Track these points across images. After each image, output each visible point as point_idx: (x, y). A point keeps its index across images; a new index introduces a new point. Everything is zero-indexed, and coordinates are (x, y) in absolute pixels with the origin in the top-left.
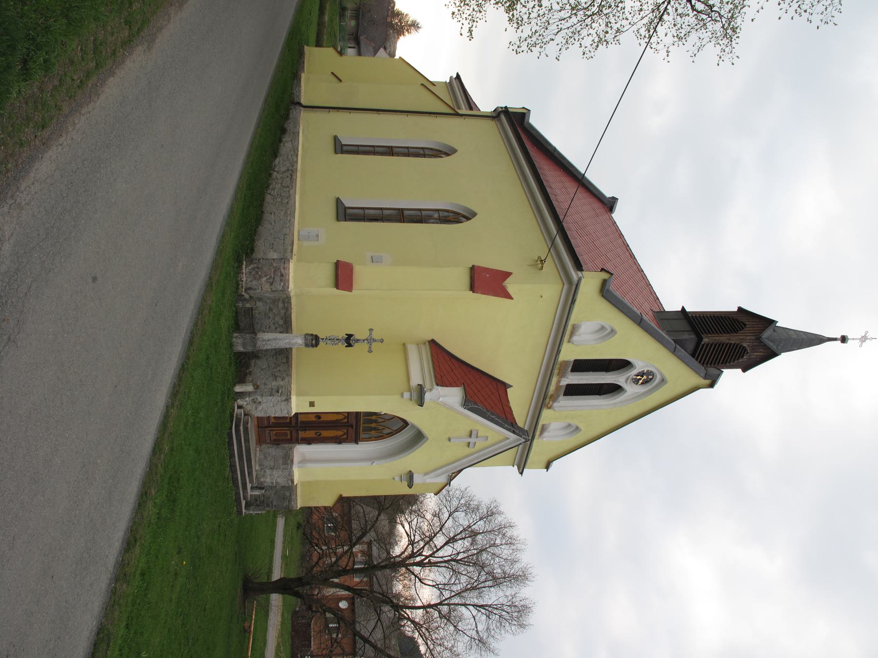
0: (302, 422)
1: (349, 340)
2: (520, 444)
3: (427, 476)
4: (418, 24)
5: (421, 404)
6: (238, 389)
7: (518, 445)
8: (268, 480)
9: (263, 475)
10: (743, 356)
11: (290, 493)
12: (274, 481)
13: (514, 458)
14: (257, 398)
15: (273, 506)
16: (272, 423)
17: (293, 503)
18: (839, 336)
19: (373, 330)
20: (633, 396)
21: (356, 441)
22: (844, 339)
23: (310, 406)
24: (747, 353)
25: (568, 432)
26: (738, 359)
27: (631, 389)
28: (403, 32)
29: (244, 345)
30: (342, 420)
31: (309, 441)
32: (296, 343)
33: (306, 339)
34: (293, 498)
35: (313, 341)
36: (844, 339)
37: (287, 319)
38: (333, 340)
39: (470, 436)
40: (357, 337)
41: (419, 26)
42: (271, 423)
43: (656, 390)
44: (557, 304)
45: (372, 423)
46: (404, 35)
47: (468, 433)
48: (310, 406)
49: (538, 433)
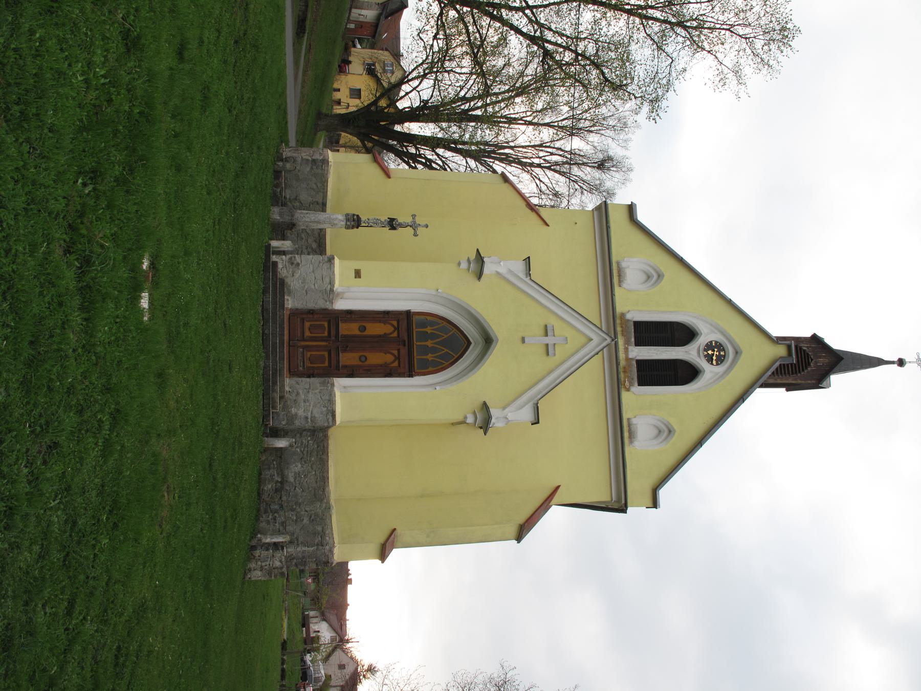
0: (344, 336)
1: (392, 224)
2: (604, 347)
3: (507, 410)
4: (374, 668)
5: (480, 275)
6: (274, 243)
7: (602, 349)
8: (301, 412)
9: (295, 400)
10: (809, 364)
11: (323, 528)
12: (309, 416)
13: (609, 486)
14: (295, 257)
15: (300, 542)
16: (307, 336)
17: (327, 538)
18: (896, 359)
19: (415, 216)
20: (715, 378)
21: (411, 376)
22: (901, 363)
23: (355, 278)
24: (812, 360)
25: (661, 440)
26: (806, 368)
27: (709, 371)
28: (360, 680)
29: (281, 214)
30: (391, 334)
31: (352, 373)
32: (337, 218)
33: (347, 220)
34: (327, 532)
35: (354, 222)
36: (901, 363)
37: (321, 241)
38: (377, 223)
39: (546, 335)
40: (401, 220)
41: (376, 669)
42: (305, 336)
43: (735, 366)
44: (593, 234)
45: (427, 327)
46: (360, 682)
47: (542, 332)
48: (355, 278)
49: (626, 441)
